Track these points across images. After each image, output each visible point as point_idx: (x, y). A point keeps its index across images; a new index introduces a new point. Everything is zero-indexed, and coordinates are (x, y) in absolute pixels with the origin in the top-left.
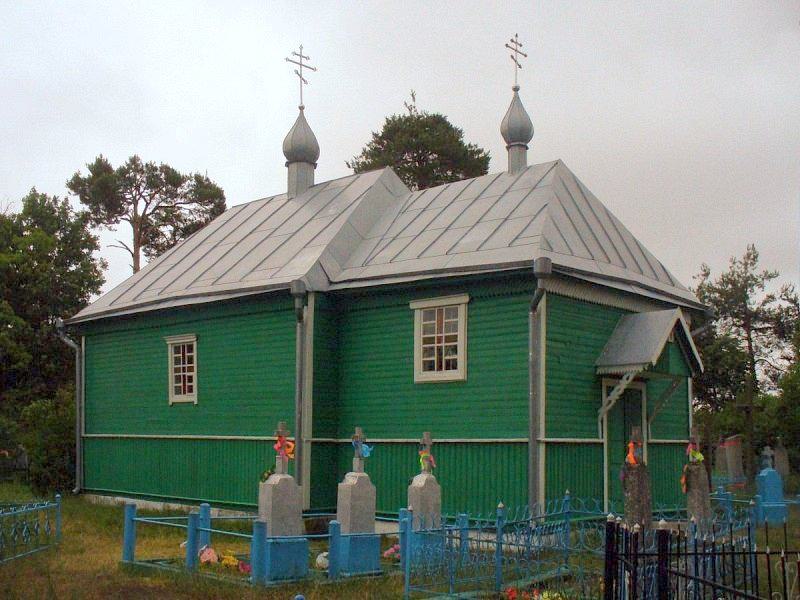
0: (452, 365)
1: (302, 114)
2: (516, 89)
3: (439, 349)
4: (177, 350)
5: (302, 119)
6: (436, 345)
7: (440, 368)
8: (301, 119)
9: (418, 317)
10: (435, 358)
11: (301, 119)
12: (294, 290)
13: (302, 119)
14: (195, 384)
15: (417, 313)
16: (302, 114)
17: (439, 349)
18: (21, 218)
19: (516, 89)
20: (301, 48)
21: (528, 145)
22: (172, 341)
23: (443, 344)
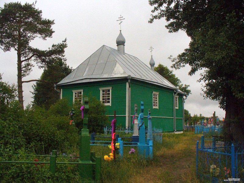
0: (109, 102)
1: (121, 32)
2: (121, 31)
3: (106, 99)
4: (103, 91)
5: (121, 34)
6: (105, 98)
7: (106, 103)
8: (121, 34)
9: (101, 92)
10: (105, 101)
11: (121, 34)
12: (128, 78)
13: (121, 34)
14: (110, 100)
15: (101, 91)
16: (121, 32)
17: (106, 99)
18: (185, 27)
19: (121, 31)
20: (121, 15)
21: (125, 44)
22: (101, 89)
23: (107, 98)
